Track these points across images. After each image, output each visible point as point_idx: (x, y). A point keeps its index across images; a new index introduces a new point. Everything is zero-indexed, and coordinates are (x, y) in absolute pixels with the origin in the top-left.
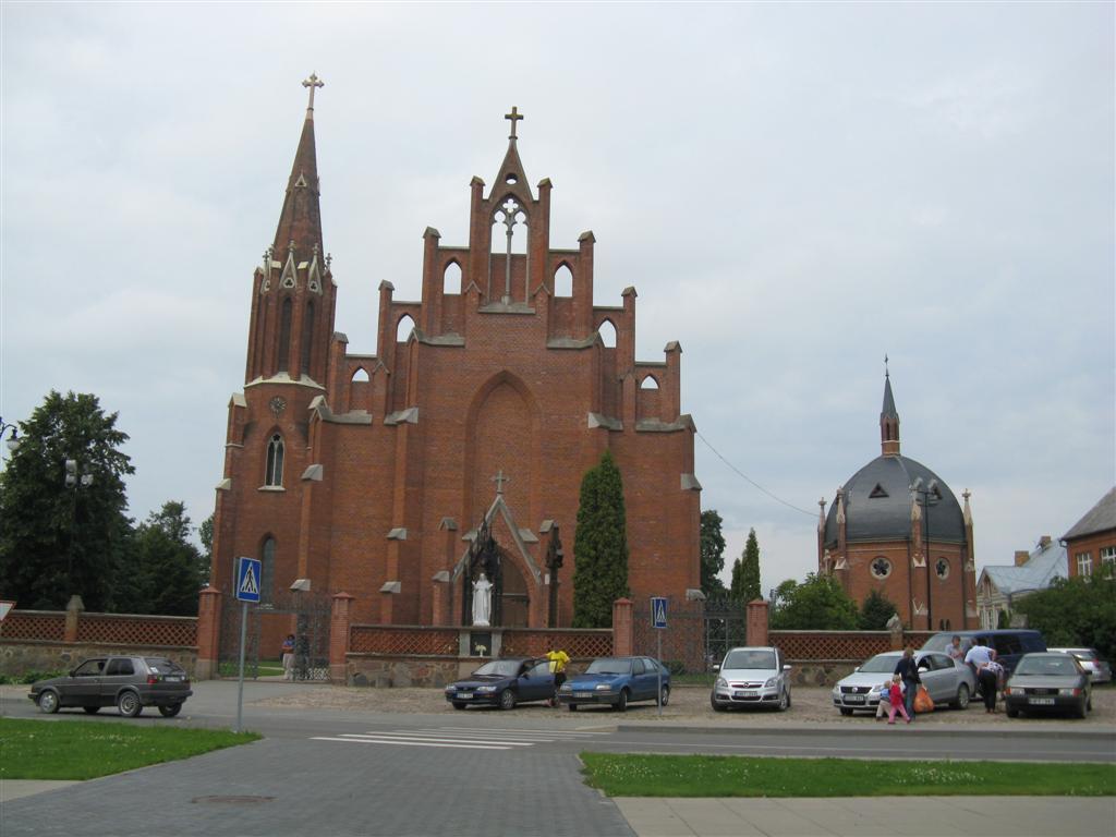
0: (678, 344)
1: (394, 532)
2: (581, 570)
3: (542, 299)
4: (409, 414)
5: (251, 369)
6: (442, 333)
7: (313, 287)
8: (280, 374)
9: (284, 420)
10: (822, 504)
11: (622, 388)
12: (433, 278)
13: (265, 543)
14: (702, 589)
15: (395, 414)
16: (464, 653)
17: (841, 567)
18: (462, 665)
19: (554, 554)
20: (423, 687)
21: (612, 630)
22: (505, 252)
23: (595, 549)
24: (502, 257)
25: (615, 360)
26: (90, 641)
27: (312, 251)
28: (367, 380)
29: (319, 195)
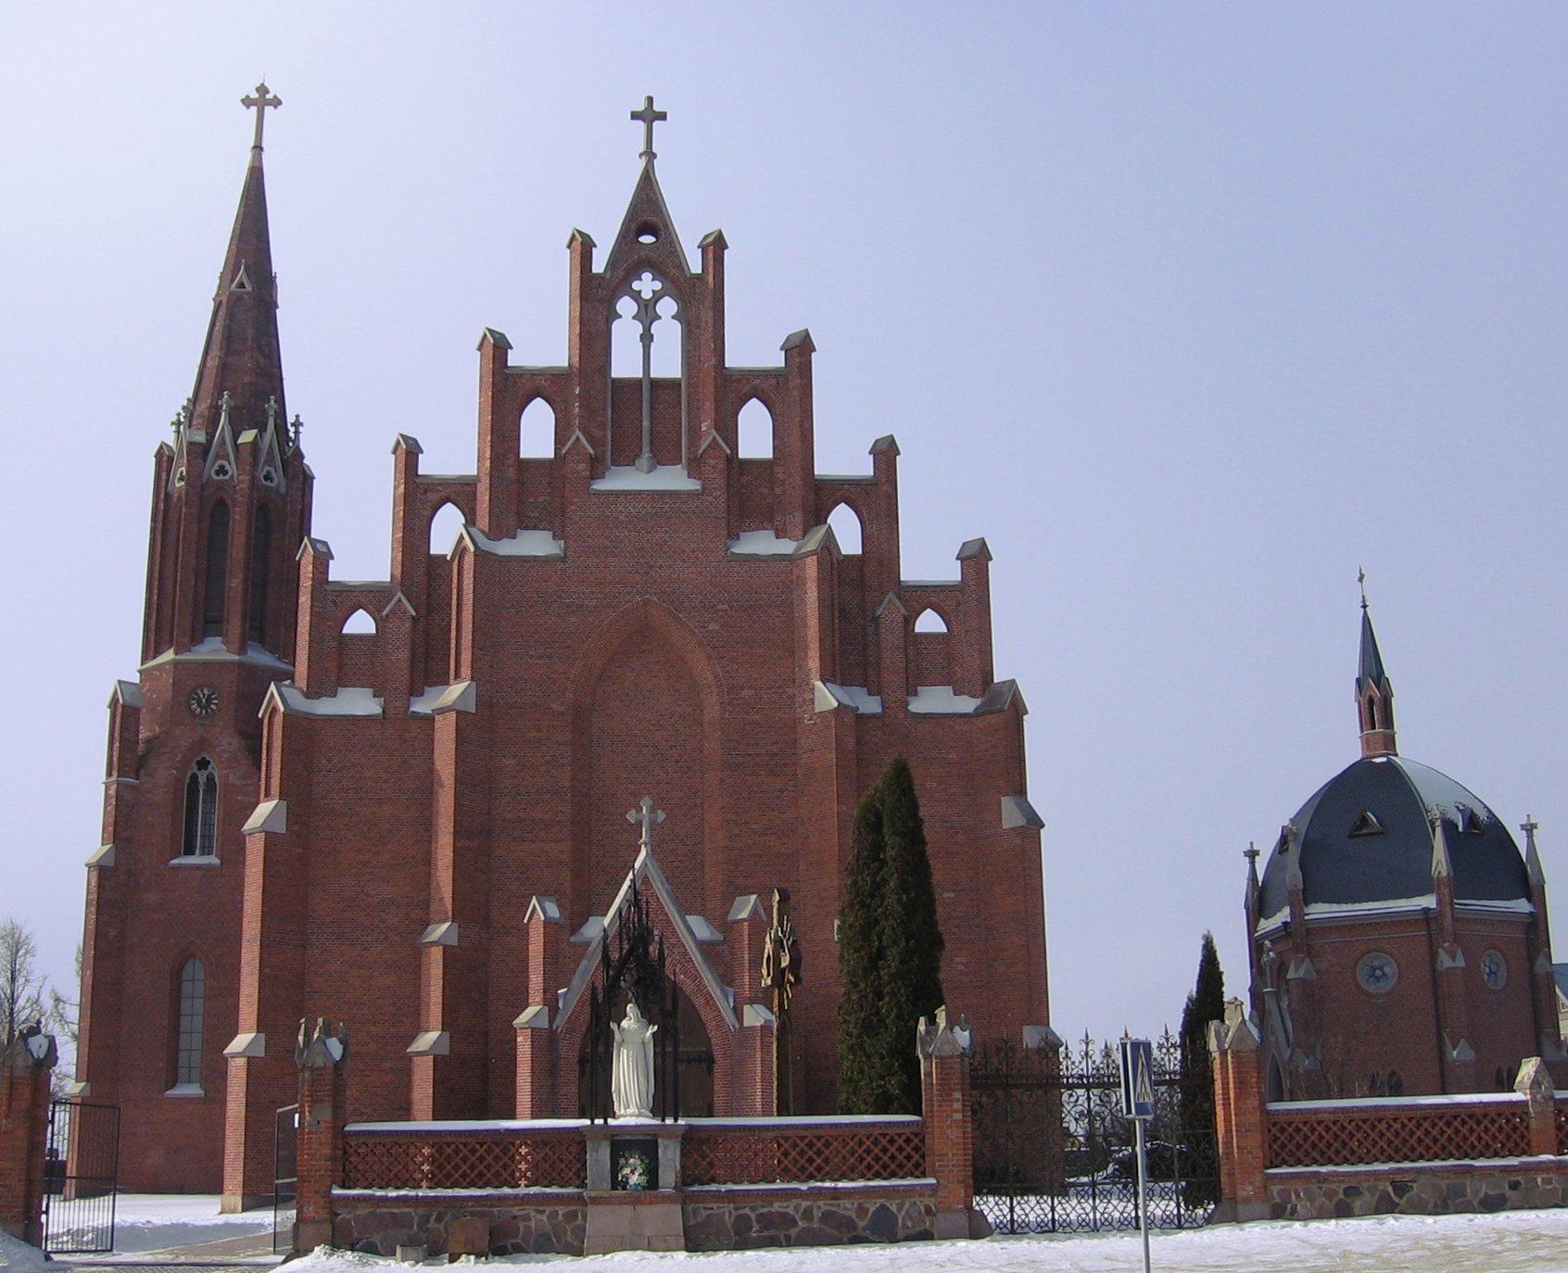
7: (267, 477)
10: (1252, 855)
17: (1301, 974)
18: (592, 1211)
22: (640, 375)
24: (634, 385)
28: (373, 630)
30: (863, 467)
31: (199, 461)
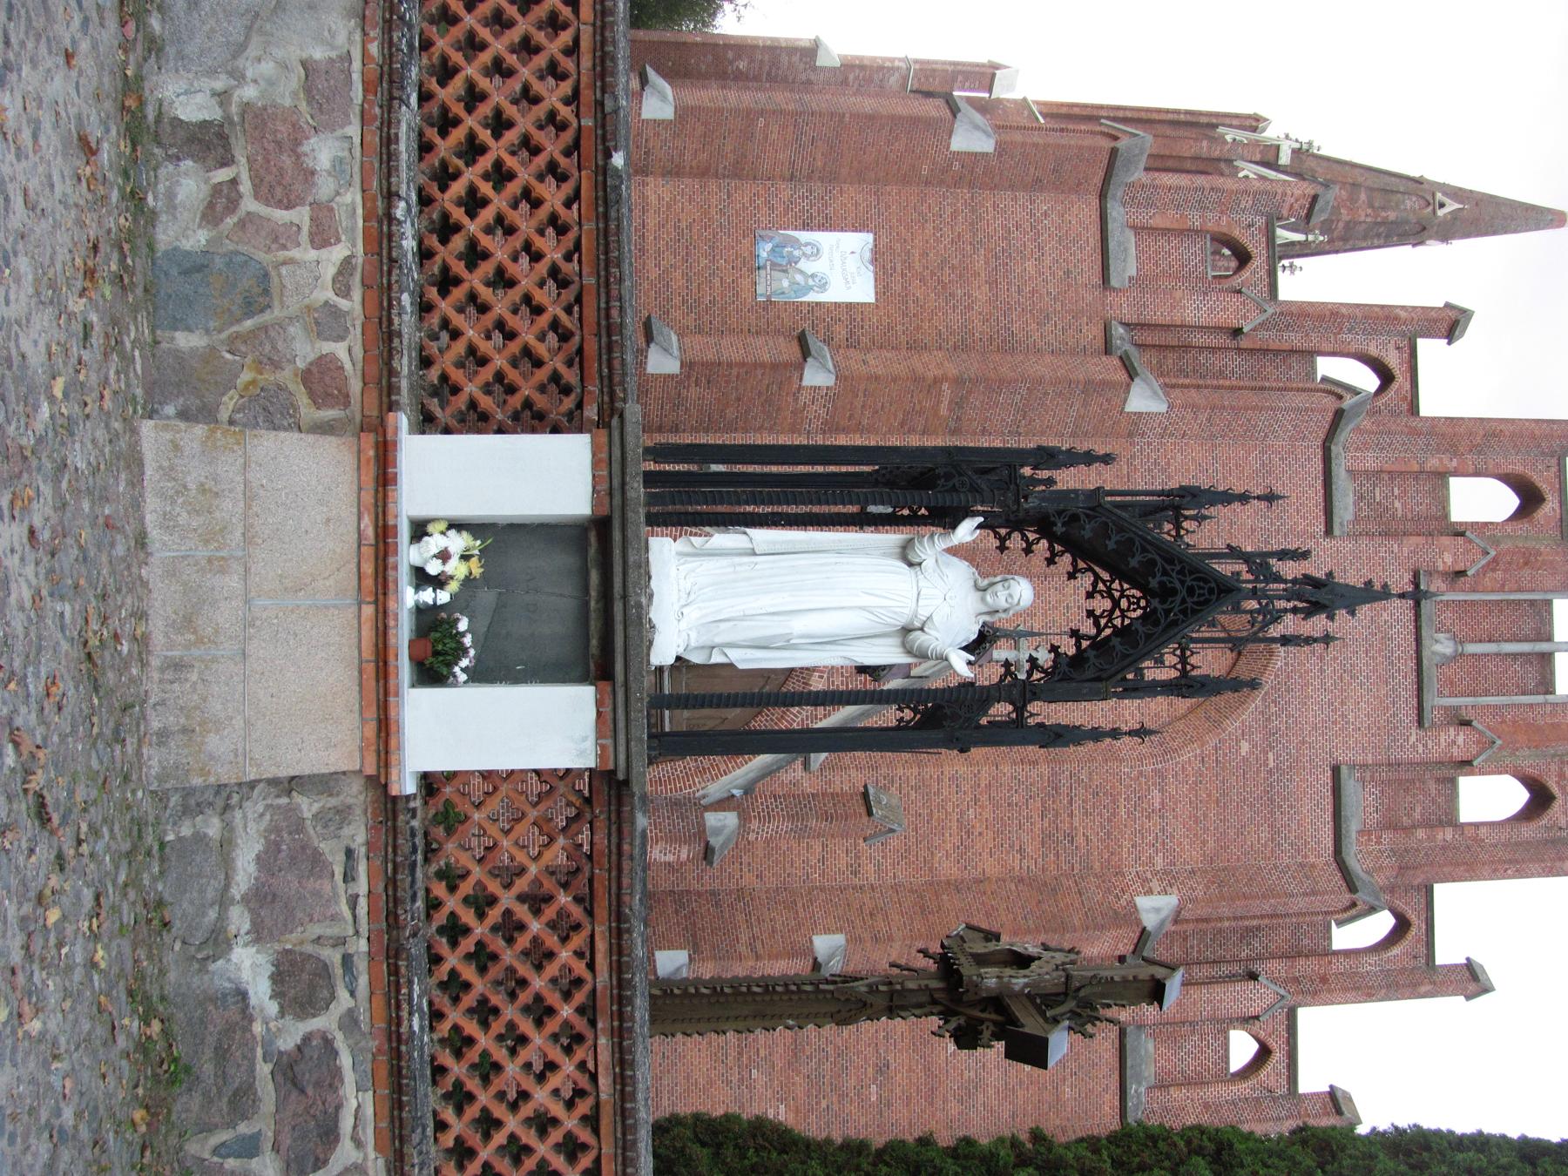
5: (1064, 110)
11: (1232, 978)
27: (1311, 231)
30: (1447, 952)
31: (1258, 157)
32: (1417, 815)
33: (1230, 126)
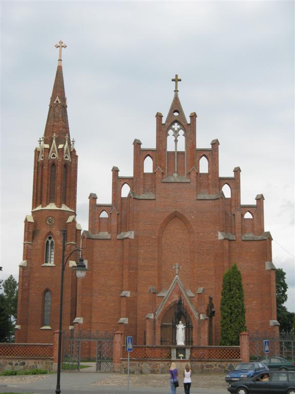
0: (262, 196)
1: (124, 293)
2: (224, 318)
3: (193, 175)
4: (130, 235)
6: (144, 192)
7: (66, 158)
8: (51, 204)
9: (54, 229)
12: (138, 166)
13: (45, 294)
14: (277, 320)
15: (122, 234)
16: (174, 358)
19: (211, 311)
20: (155, 373)
21: (239, 347)
22: (174, 150)
23: (231, 309)
25: (231, 204)
26: (4, 356)
29: (67, 107)
32: (206, 181)
33: (38, 158)
